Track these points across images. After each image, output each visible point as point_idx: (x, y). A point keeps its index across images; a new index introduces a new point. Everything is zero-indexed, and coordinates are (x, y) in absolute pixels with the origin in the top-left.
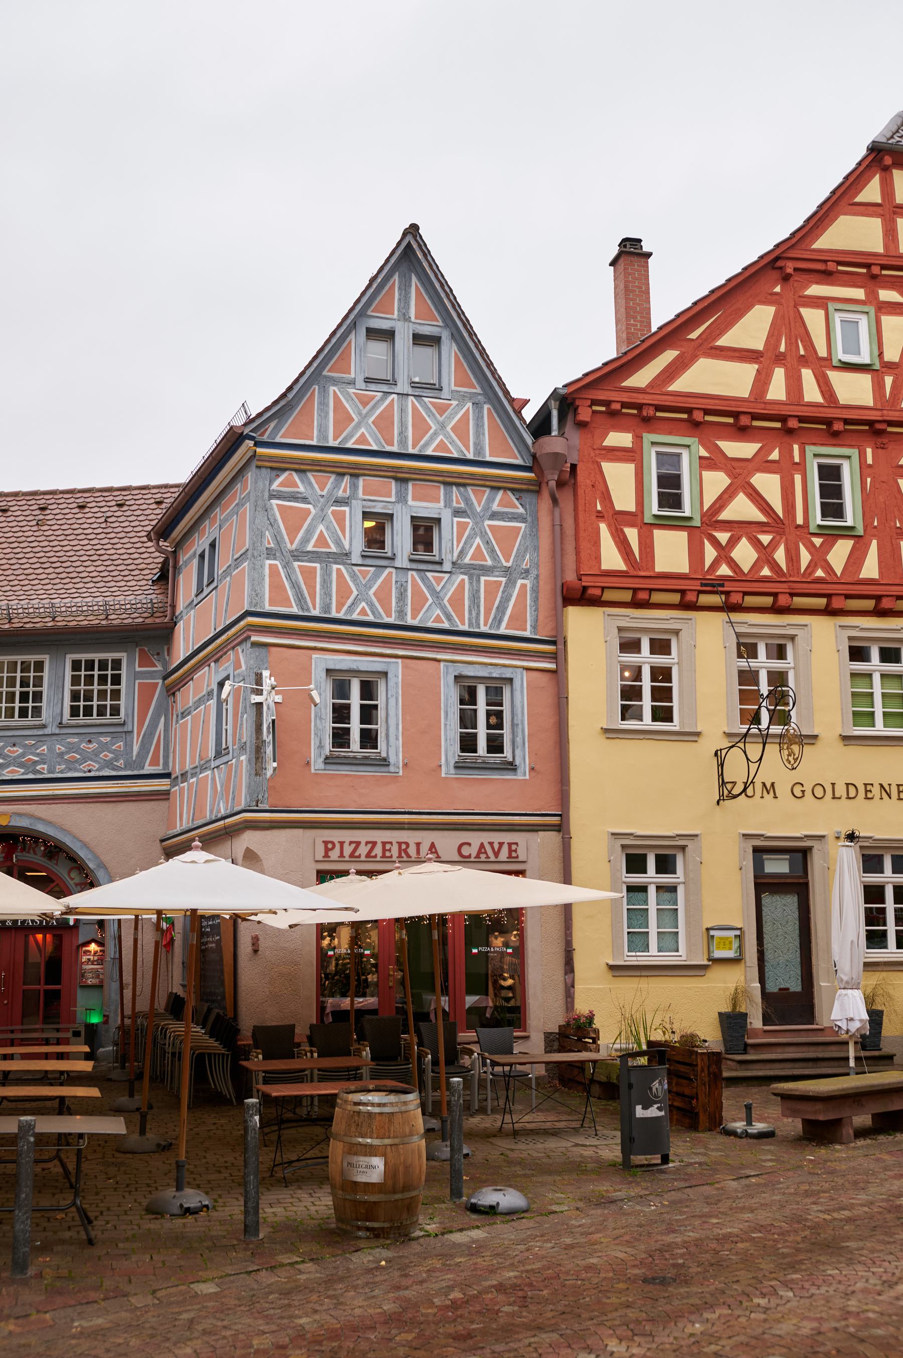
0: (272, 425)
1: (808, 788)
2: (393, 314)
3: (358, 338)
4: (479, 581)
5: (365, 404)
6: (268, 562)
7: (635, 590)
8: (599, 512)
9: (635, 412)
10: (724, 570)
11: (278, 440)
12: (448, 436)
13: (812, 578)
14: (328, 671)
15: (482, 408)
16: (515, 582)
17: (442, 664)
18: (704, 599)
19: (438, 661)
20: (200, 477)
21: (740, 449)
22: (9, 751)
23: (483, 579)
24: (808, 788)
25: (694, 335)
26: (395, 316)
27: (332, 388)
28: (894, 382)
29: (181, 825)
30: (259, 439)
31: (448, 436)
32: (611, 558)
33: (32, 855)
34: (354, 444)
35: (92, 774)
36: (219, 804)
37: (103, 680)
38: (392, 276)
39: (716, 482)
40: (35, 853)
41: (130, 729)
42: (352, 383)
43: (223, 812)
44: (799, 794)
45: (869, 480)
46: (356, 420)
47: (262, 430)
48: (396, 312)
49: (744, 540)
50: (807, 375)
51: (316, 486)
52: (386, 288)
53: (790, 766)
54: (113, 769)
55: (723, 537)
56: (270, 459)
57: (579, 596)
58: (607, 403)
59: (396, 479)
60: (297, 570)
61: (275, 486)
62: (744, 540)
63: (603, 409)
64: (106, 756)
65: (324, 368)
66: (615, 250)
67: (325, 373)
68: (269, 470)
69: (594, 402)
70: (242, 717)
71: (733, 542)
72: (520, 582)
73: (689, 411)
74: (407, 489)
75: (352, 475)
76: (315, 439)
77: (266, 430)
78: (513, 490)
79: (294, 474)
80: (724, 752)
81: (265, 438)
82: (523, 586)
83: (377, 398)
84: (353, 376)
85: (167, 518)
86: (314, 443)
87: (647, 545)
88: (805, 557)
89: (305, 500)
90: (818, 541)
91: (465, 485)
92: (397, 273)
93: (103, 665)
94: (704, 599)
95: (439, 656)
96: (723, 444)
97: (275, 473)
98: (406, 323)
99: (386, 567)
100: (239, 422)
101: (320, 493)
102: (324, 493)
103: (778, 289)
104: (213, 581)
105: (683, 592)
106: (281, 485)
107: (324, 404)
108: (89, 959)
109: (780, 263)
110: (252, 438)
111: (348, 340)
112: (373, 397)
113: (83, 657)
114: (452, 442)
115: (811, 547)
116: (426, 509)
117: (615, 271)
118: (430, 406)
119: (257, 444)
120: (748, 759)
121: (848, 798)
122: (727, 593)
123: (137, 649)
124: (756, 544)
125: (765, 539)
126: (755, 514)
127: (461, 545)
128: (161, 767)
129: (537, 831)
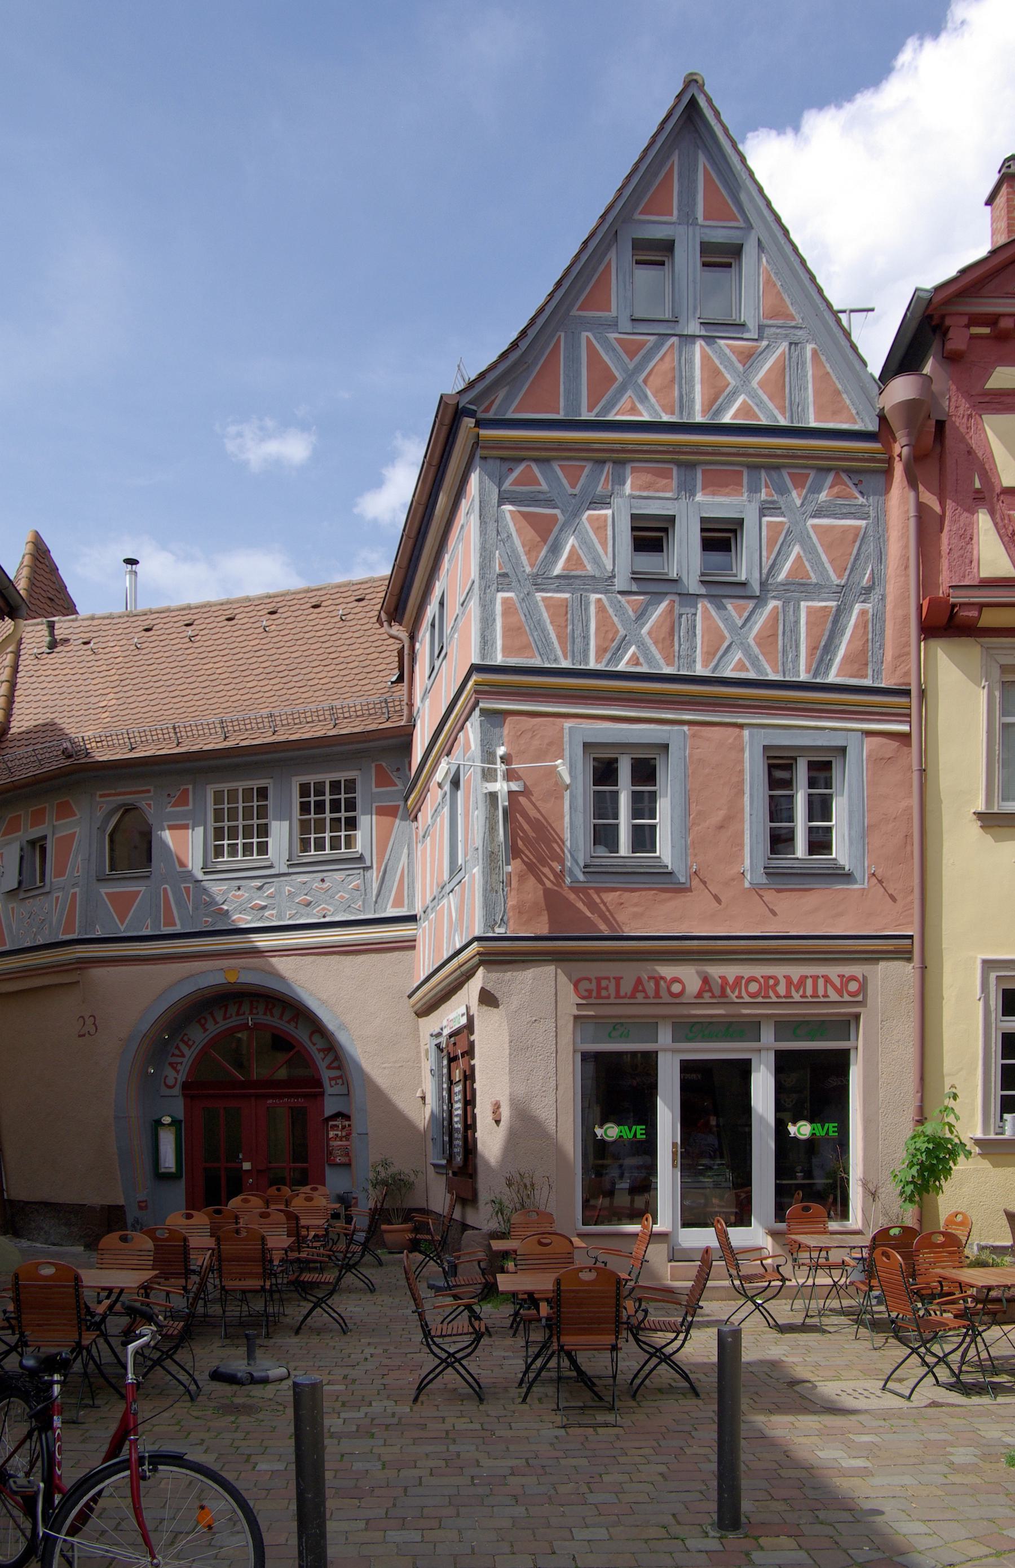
0: (502, 394)
2: (671, 215)
3: (619, 259)
5: (632, 355)
6: (500, 595)
8: (977, 491)
11: (510, 415)
12: (753, 395)
14: (586, 745)
15: (803, 349)
16: (851, 608)
17: (746, 733)
19: (741, 726)
22: (234, 895)
23: (803, 604)
26: (674, 218)
30: (480, 415)
31: (753, 395)
33: (268, 1017)
35: (327, 920)
37: (335, 807)
40: (272, 1015)
41: (368, 864)
42: (614, 324)
46: (620, 379)
47: (486, 404)
48: (675, 212)
51: (565, 481)
54: (351, 913)
56: (498, 444)
58: (992, 320)
59: (679, 464)
60: (541, 604)
61: (506, 485)
63: (987, 330)
64: (342, 897)
65: (572, 305)
67: (574, 312)
68: (498, 462)
69: (976, 320)
70: (473, 813)
72: (858, 607)
74: (694, 479)
75: (615, 462)
76: (562, 412)
77: (492, 402)
78: (849, 472)
79: (534, 466)
81: (490, 415)
82: (863, 612)
83: (649, 345)
84: (614, 313)
86: (561, 416)
89: (549, 503)
91: (777, 468)
92: (677, 152)
93: (335, 786)
95: (740, 721)
97: (506, 466)
98: (691, 228)
101: (571, 491)
102: (576, 491)
106: (516, 482)
107: (573, 360)
108: (337, 1135)
110: (472, 414)
112: (643, 344)
113: (312, 779)
116: (721, 504)
117: (992, 211)
119: (479, 424)
123: (373, 765)
127: (773, 557)
128: (405, 909)
129: (878, 959)
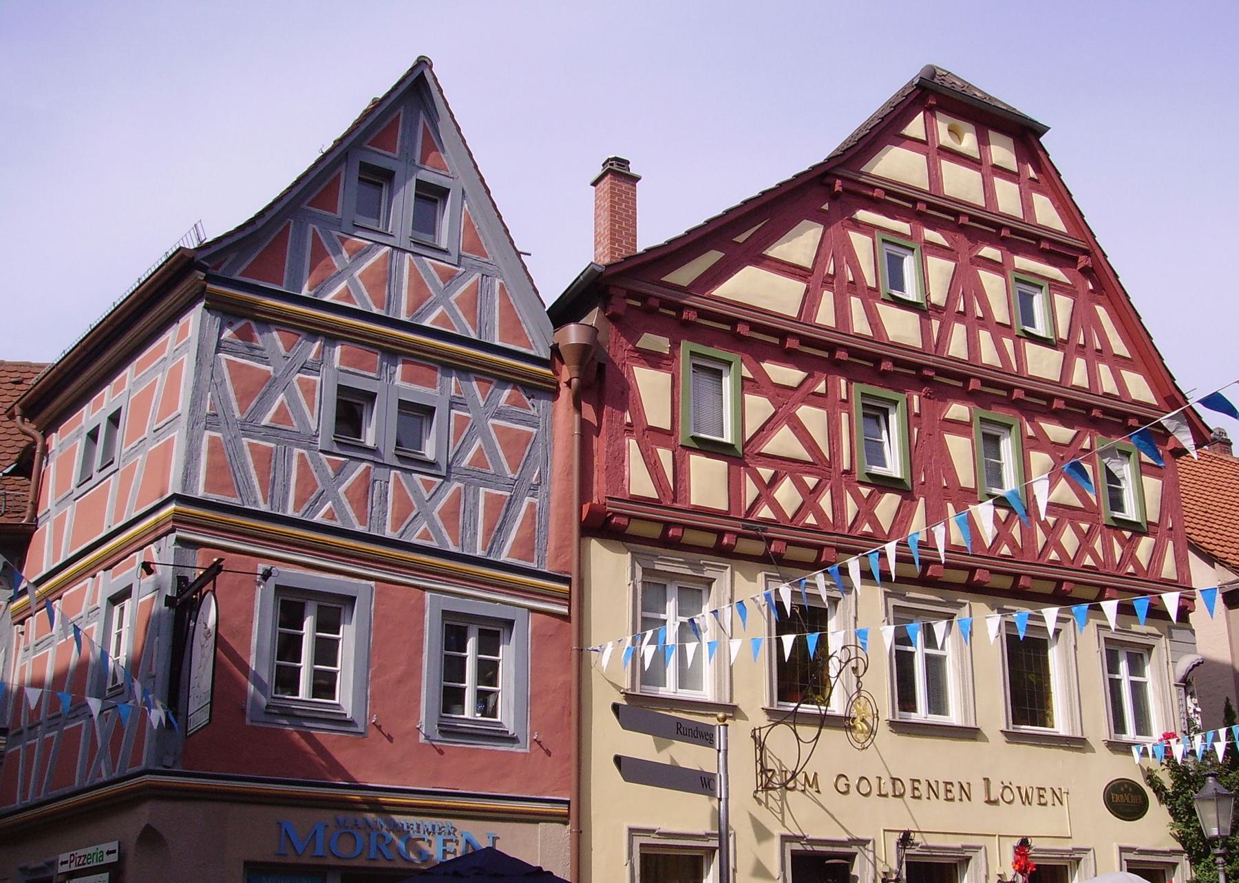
0: (232, 256)
1: (854, 782)
4: (476, 493)
6: (207, 433)
7: (668, 525)
9: (673, 313)
10: (765, 512)
13: (859, 532)
18: (745, 546)
19: (424, 589)
20: (60, 371)
21: (785, 374)
24: (854, 782)
25: (741, 239)
27: (311, 226)
28: (941, 327)
29: (25, 797)
32: (640, 483)
34: (336, 298)
36: (98, 764)
38: (336, 167)
39: (759, 408)
43: (105, 777)
44: (843, 788)
45: (916, 430)
49: (788, 480)
50: (856, 303)
52: (390, 120)
53: (859, 746)
55: (766, 473)
57: (600, 526)
58: (643, 298)
62: (788, 480)
66: (599, 171)
71: (775, 480)
72: (527, 500)
73: (734, 322)
77: (222, 263)
80: (764, 732)
81: (219, 273)
84: (339, 215)
85: (43, 386)
87: (680, 468)
88: (851, 508)
90: (865, 491)
94: (745, 546)
96: (768, 367)
99: (363, 460)
100: (192, 244)
103: (826, 207)
104: (112, 462)
105: (721, 533)
109: (827, 180)
110: (203, 269)
111: (337, 172)
114: (456, 316)
115: (857, 497)
116: (419, 393)
118: (432, 269)
119: (209, 278)
120: (798, 738)
121: (895, 796)
122: (770, 540)
124: (800, 485)
125: (811, 481)
126: (798, 451)
129: (537, 822)
